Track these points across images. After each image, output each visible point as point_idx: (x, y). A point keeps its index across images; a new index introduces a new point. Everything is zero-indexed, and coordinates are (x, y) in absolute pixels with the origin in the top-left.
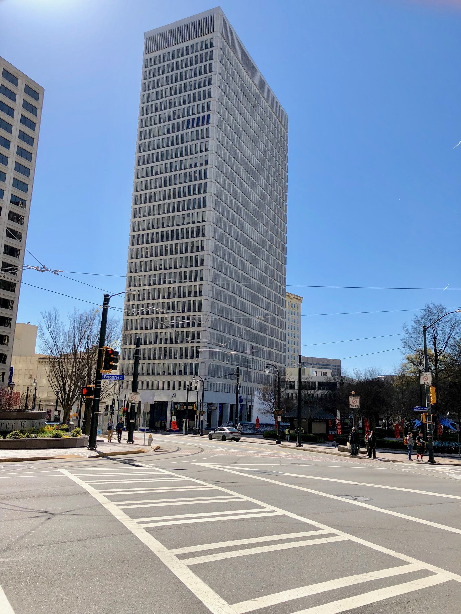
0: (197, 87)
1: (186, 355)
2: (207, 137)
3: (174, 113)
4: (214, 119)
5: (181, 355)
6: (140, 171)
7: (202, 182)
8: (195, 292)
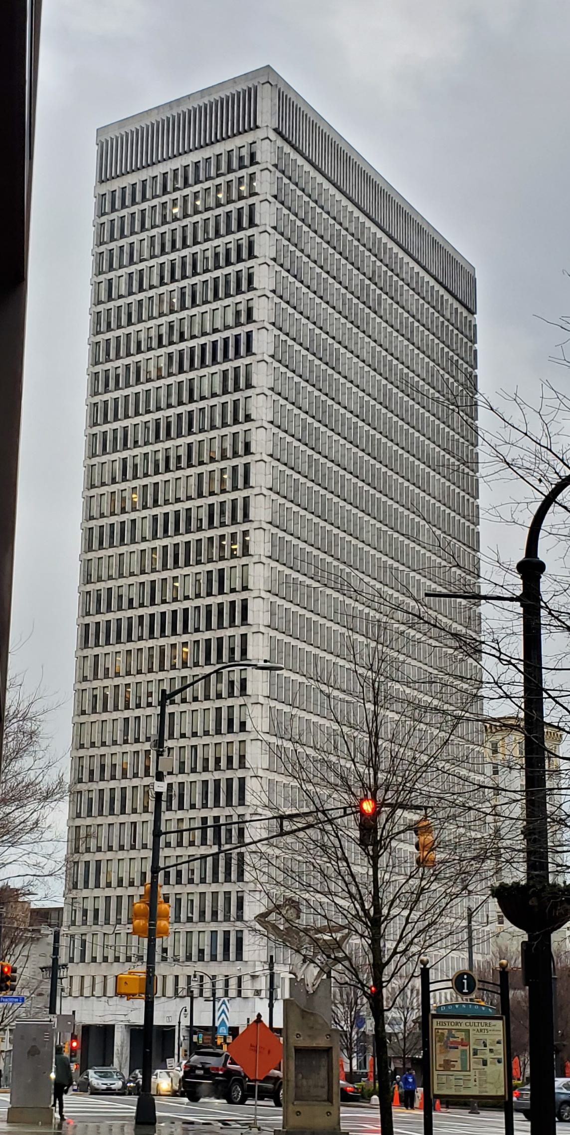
0: (222, 262)
1: (215, 914)
2: (249, 386)
3: (171, 327)
4: (263, 343)
5: (202, 913)
6: (97, 470)
7: (239, 495)
8: (230, 759)
